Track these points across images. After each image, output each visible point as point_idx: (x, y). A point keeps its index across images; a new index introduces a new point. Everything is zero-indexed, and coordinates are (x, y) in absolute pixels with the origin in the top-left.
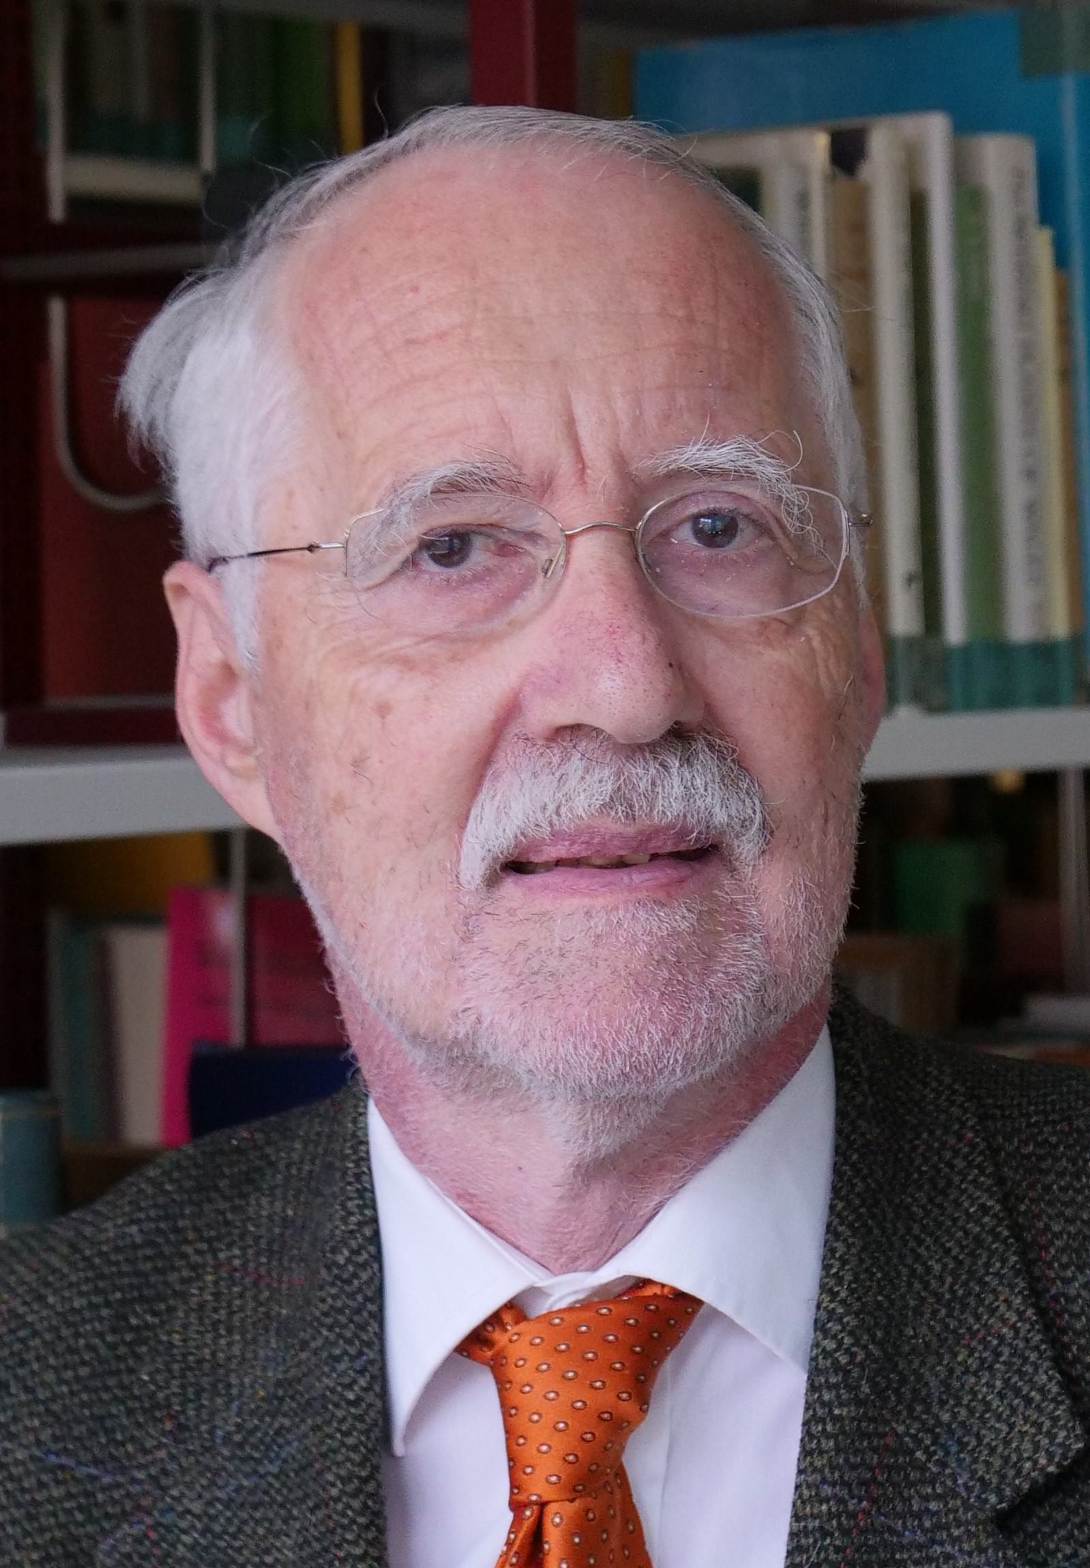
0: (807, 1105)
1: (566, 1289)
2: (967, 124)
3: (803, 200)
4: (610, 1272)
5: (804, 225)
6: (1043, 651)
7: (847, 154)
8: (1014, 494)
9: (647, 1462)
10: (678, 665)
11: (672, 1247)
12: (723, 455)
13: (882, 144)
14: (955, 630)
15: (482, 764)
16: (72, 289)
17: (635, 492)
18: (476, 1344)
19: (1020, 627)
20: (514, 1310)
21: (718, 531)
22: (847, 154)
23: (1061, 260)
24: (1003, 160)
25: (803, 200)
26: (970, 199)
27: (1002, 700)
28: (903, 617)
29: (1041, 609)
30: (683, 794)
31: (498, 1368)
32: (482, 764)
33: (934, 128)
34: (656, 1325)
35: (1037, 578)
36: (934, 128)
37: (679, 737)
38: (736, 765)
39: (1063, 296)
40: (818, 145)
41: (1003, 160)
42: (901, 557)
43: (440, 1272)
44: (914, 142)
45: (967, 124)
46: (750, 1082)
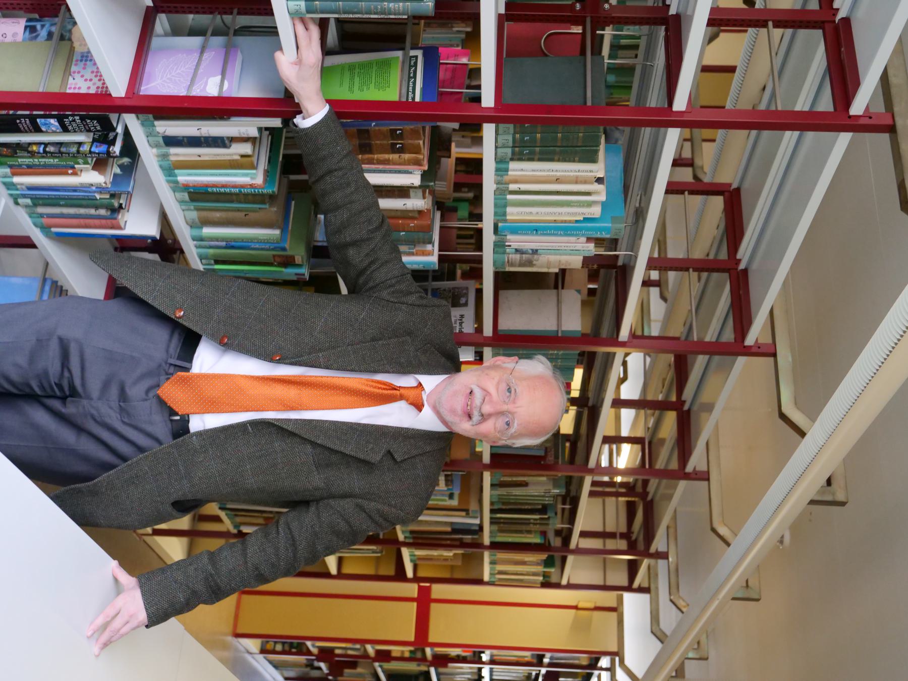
0: (441, 428)
1: (425, 397)
2: (604, 205)
3: (591, 171)
4: (425, 403)
5: (587, 171)
6: (505, 214)
7: (599, 180)
8: (534, 210)
9: (402, 404)
10: (490, 415)
11: (427, 409)
12: (515, 424)
13: (601, 188)
14: (509, 197)
15: (484, 390)
16: (583, 34)
17: (512, 413)
18: (420, 384)
19: (509, 210)
20: (423, 389)
21: (508, 424)
22: (599, 180)
23: (577, 221)
24: (596, 211)
25: (591, 171)
26: (590, 204)
27: (496, 205)
28: (512, 187)
29: (512, 214)
30: (476, 417)
31: (416, 387)
32: (484, 390)
33: (603, 198)
34: (419, 407)
35: (518, 214)
36: (603, 198)
37: (482, 415)
38: (480, 423)
39: (570, 222)
40: (601, 175)
41: (596, 211)
42: (524, 187)
43: (430, 382)
44: (601, 193)
45: (604, 205)
46: (444, 422)
